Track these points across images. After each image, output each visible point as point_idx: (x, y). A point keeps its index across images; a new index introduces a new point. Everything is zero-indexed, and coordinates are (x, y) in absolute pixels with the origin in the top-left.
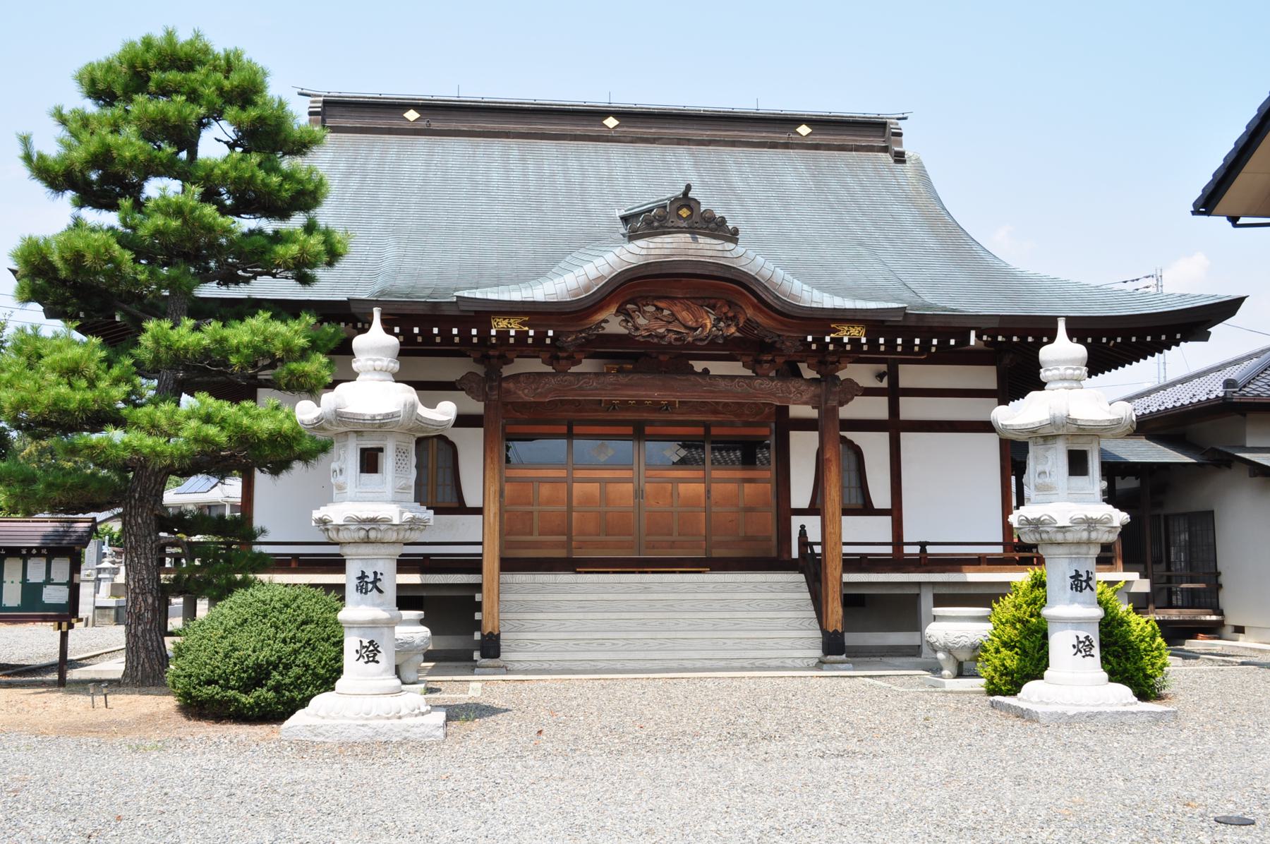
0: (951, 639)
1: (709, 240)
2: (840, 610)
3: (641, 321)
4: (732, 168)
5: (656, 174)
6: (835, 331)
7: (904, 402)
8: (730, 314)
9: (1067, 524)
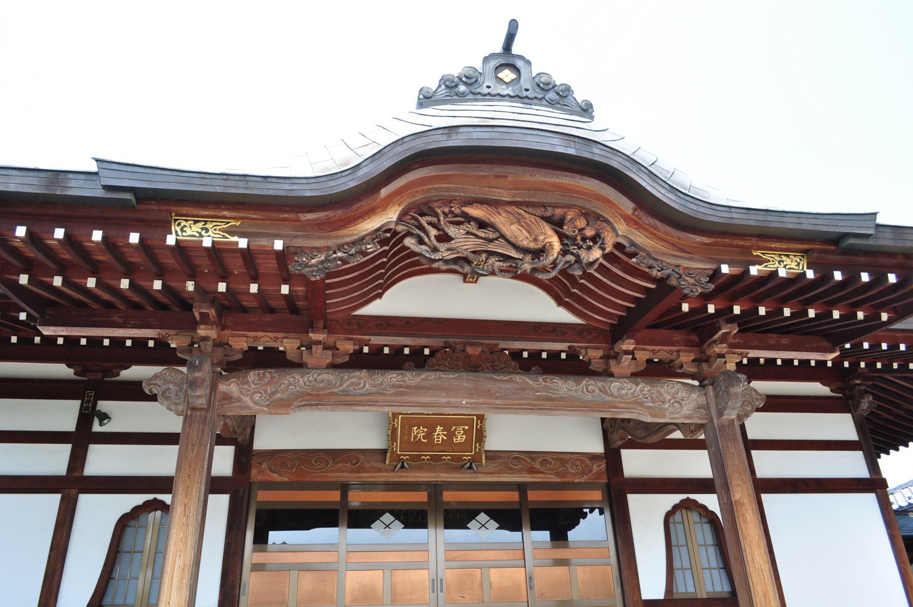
8: (589, 233)
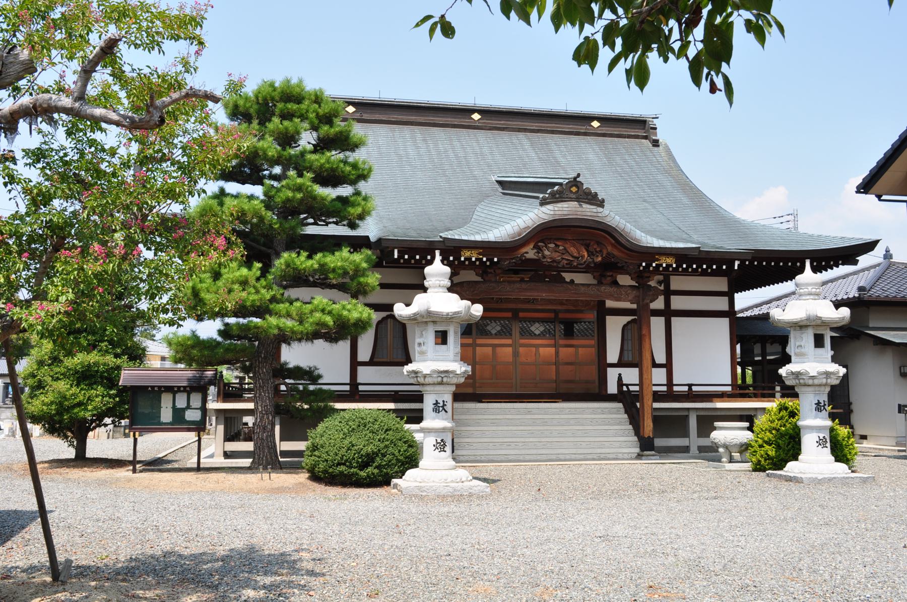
0: (728, 440)
1: (588, 206)
2: (651, 424)
3: (547, 253)
4: (554, 147)
5: (536, 158)
6: (658, 260)
7: (674, 299)
9: (815, 374)
